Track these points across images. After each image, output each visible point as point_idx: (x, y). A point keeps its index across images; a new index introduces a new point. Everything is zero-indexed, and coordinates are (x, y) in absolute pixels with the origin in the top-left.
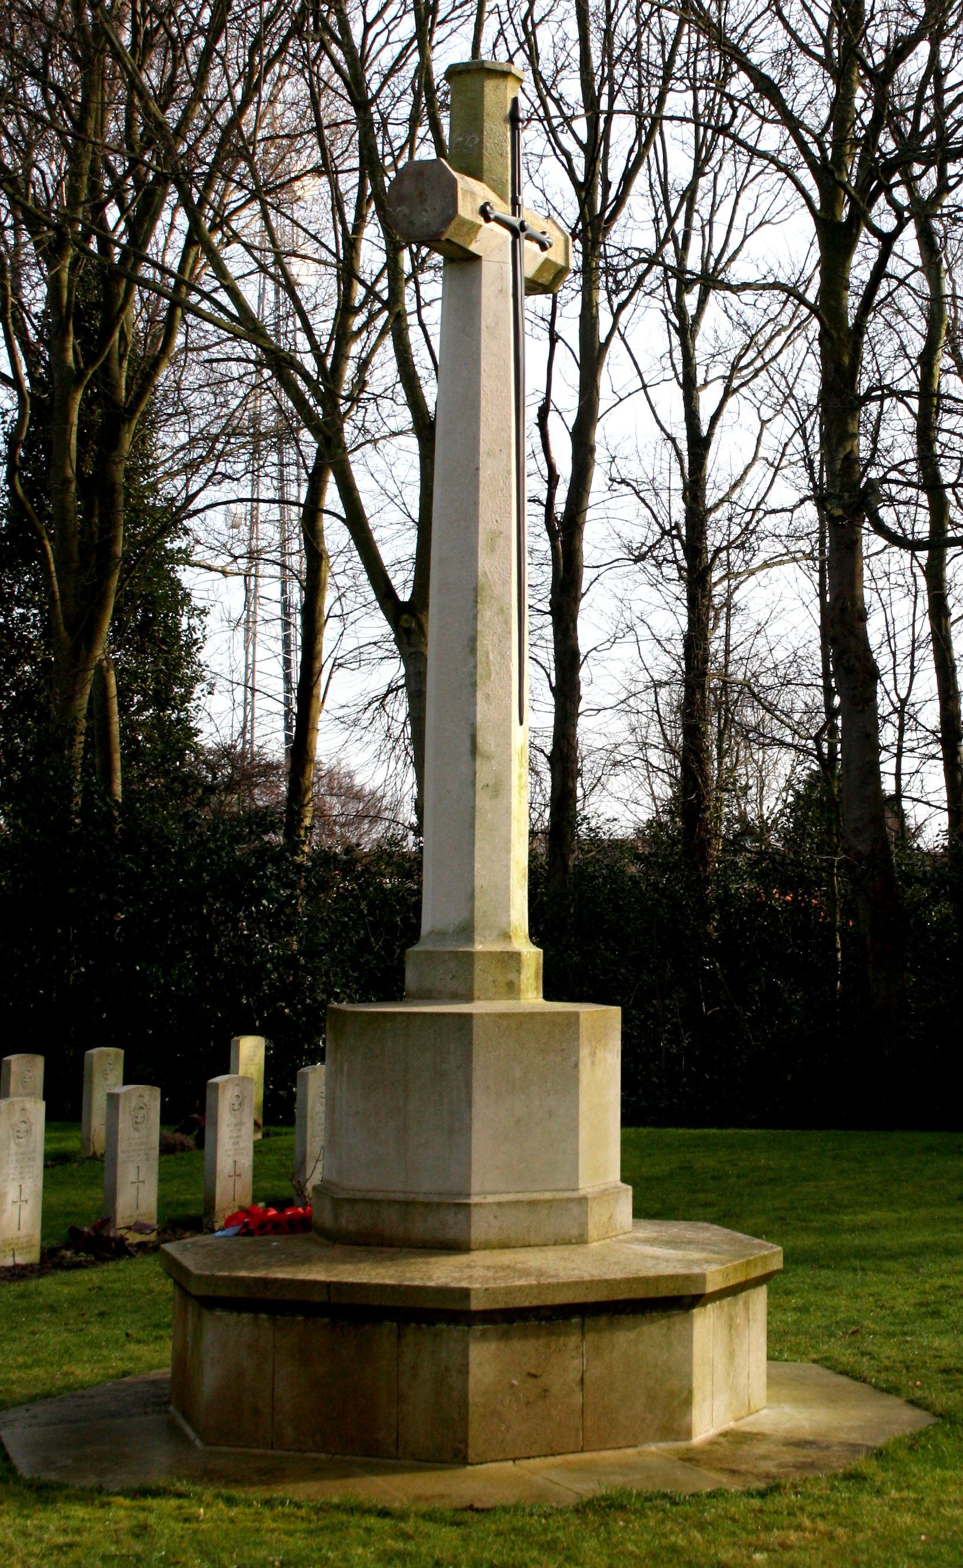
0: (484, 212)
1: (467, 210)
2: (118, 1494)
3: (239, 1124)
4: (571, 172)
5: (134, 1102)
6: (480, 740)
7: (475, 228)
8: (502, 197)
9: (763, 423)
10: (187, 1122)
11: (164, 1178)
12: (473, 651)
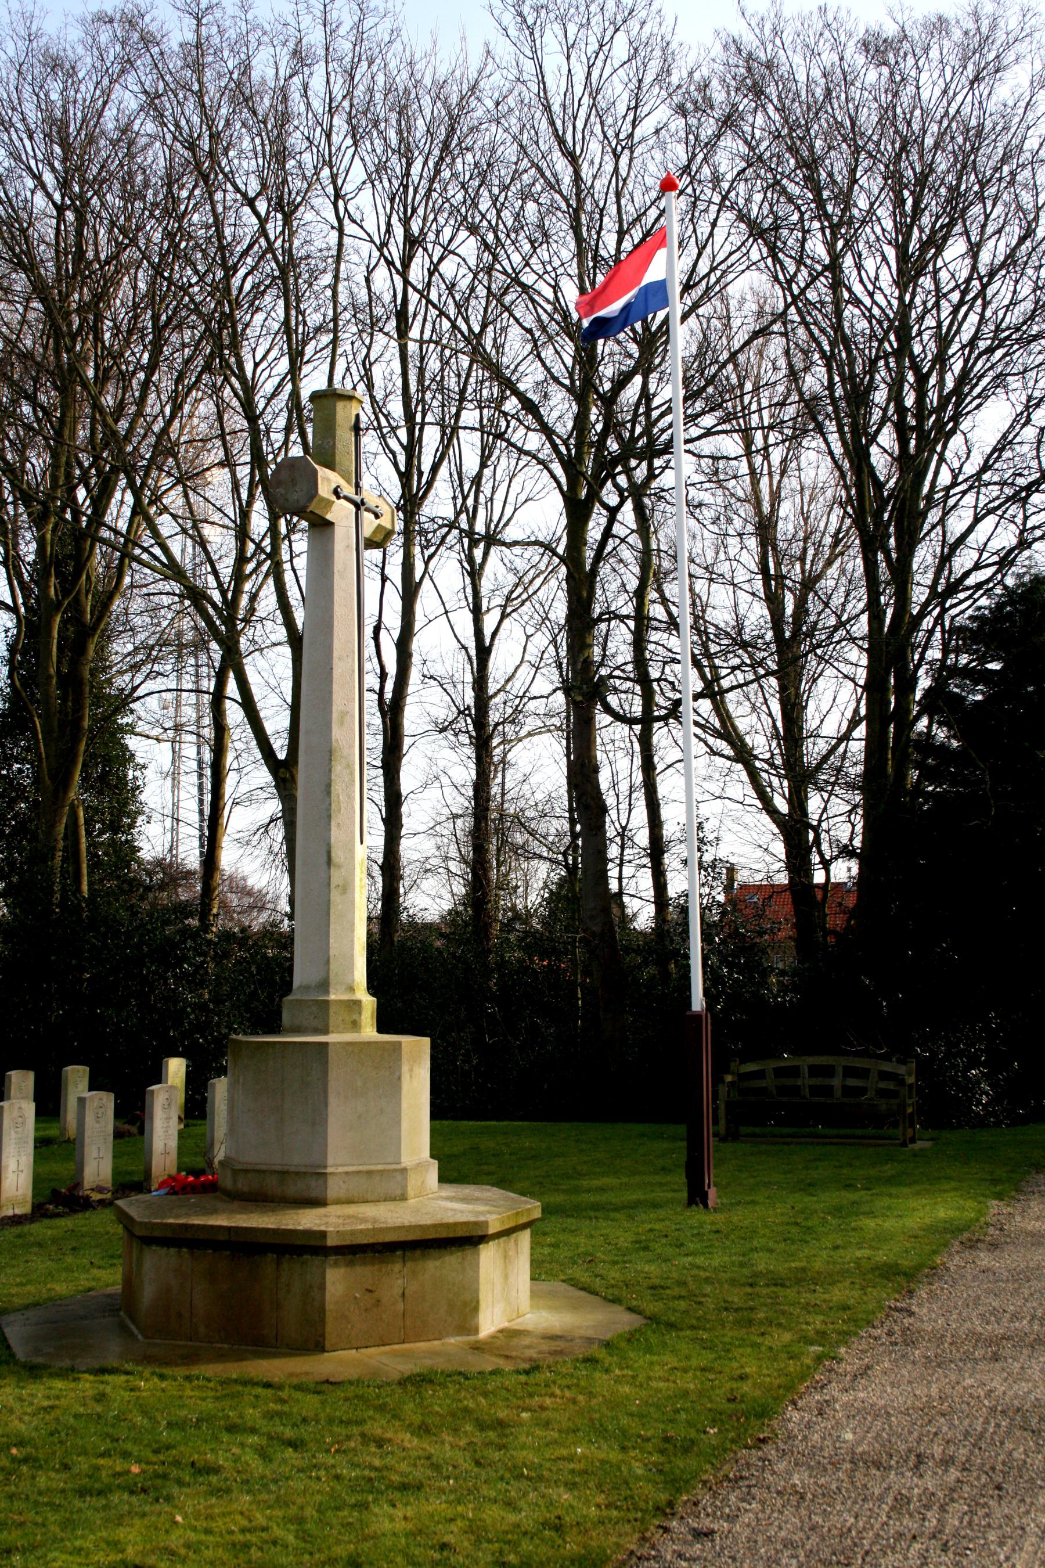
0: (336, 492)
4: (396, 465)
7: (330, 503)
8: (349, 482)
9: (528, 637)
10: (132, 1117)
12: (329, 793)
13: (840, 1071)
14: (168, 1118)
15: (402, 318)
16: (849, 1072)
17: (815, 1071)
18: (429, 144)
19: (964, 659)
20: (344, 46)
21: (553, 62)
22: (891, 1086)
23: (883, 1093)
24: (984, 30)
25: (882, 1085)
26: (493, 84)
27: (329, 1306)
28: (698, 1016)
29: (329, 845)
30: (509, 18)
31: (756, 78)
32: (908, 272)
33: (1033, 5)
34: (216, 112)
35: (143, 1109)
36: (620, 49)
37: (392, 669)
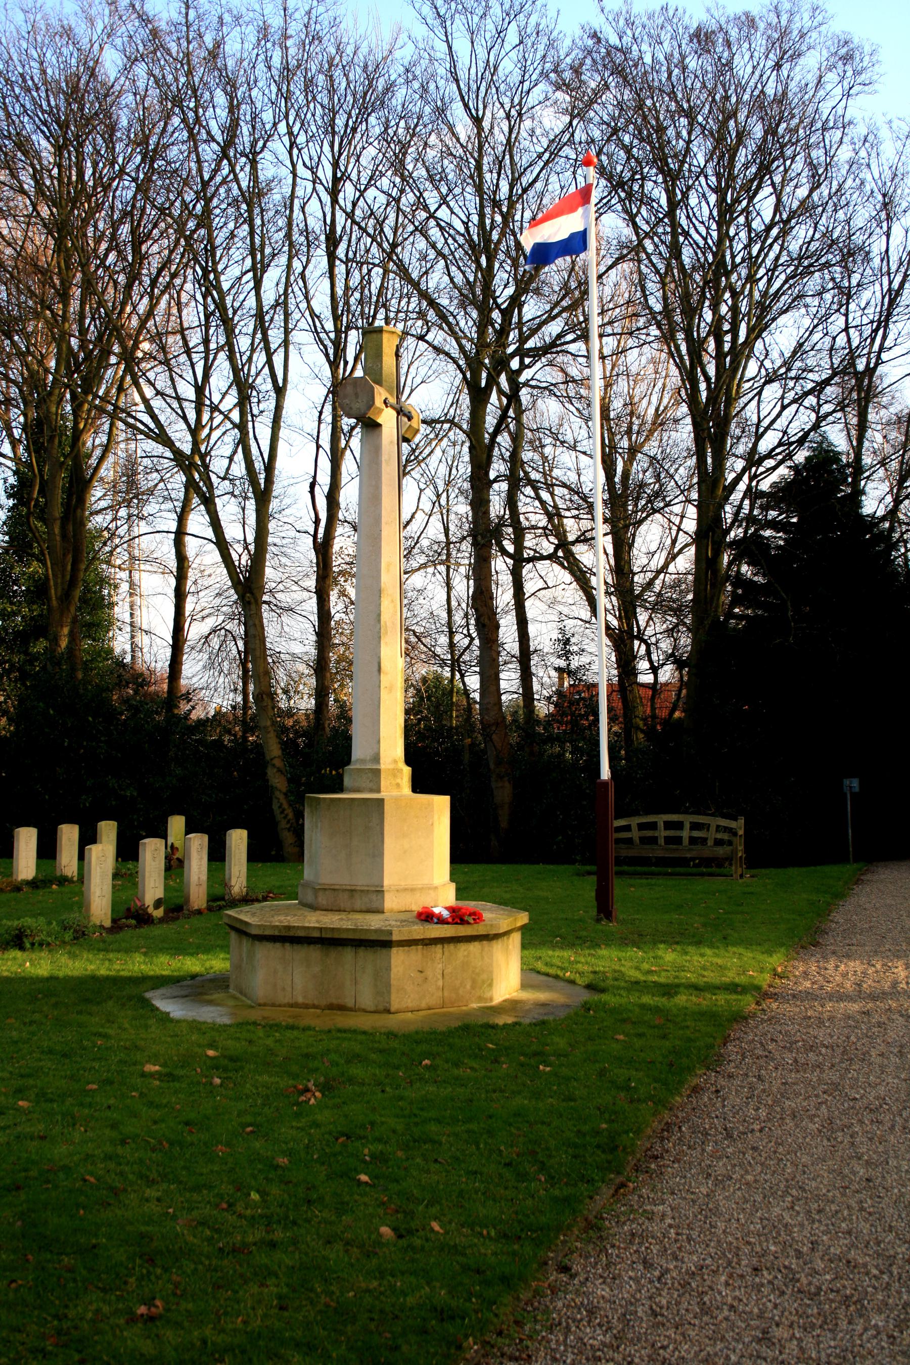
0: (385, 402)
1: (379, 402)
2: (230, 1026)
3: (201, 859)
4: (327, 355)
5: (153, 847)
6: (382, 665)
7: (380, 411)
8: (391, 395)
9: (421, 490)
10: (217, 854)
11: (249, 877)
12: (379, 621)
13: (687, 826)
14: (201, 859)
15: (332, 241)
16: (695, 826)
17: (668, 825)
18: (348, 101)
19: (772, 514)
20: (294, 28)
21: (462, 46)
22: (725, 836)
23: (719, 843)
24: (784, 22)
25: (719, 836)
26: (405, 54)
27: (393, 982)
28: (605, 783)
29: (379, 658)
30: (427, 10)
31: (618, 65)
32: (725, 214)
33: (821, 4)
34: (187, 72)
35: (12, 867)
36: (512, 37)
37: (323, 516)
